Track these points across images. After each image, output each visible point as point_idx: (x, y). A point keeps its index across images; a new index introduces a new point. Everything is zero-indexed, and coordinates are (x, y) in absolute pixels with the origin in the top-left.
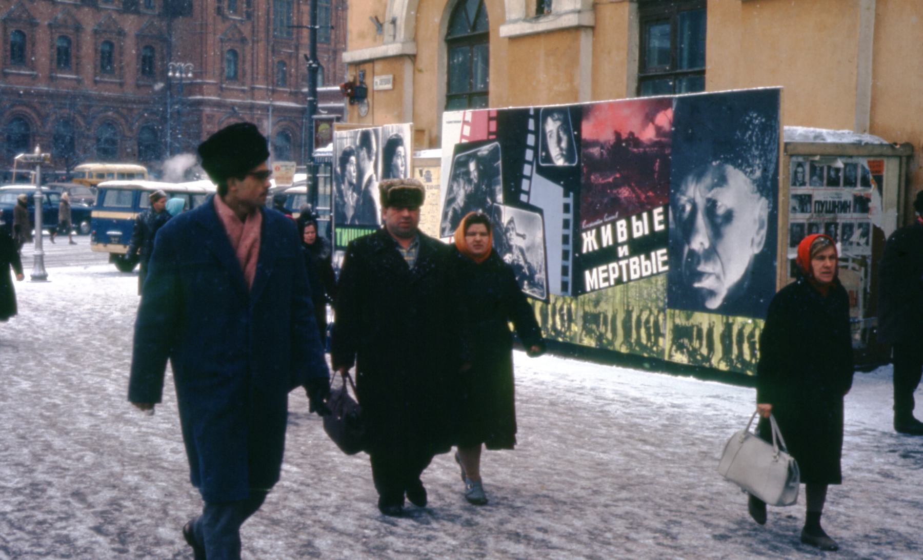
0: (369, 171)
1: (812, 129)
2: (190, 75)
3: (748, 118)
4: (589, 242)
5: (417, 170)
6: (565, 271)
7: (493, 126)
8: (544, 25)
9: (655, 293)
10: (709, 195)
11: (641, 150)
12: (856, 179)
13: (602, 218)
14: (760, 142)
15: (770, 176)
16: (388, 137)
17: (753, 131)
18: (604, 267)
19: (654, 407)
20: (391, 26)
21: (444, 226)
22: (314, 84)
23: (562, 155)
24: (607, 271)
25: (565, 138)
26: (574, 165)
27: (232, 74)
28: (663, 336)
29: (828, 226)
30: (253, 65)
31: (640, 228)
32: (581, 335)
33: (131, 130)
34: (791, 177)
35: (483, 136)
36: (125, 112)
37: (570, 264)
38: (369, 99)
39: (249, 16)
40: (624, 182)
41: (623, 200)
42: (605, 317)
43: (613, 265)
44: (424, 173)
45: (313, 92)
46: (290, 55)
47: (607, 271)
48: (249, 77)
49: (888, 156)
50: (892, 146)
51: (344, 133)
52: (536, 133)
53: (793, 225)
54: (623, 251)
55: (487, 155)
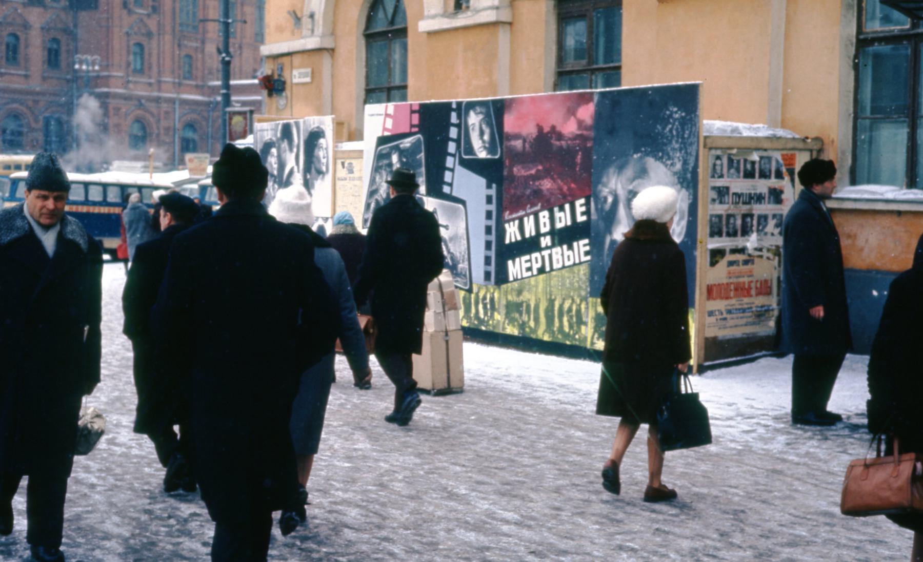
0: (290, 163)
1: (729, 123)
2: (97, 68)
3: (668, 112)
4: (512, 233)
5: (339, 162)
6: (487, 261)
7: (416, 119)
8: (462, 20)
9: (578, 282)
10: (631, 187)
11: (563, 143)
12: (770, 171)
13: (525, 209)
14: (681, 135)
15: (690, 169)
16: (310, 129)
17: (673, 124)
18: (527, 257)
19: (581, 393)
20: (309, 20)
21: (366, 217)
22: (227, 76)
23: (485, 148)
24: (530, 261)
25: (487, 131)
26: (497, 157)
27: (139, 67)
28: (586, 324)
29: (744, 217)
30: (159, 58)
31: (563, 219)
32: (504, 323)
33: (36, 121)
34: (710, 170)
35: (406, 129)
36: (30, 103)
37: (492, 254)
38: (287, 92)
39: (155, 10)
40: (547, 173)
41: (545, 192)
42: (528, 306)
43: (535, 255)
44: (346, 165)
45: (227, 86)
46: (196, 49)
47: (530, 261)
48: (155, 69)
49: (800, 150)
50: (804, 140)
51: (265, 125)
52: (458, 126)
53: (712, 216)
54: (545, 241)
55: (410, 147)
